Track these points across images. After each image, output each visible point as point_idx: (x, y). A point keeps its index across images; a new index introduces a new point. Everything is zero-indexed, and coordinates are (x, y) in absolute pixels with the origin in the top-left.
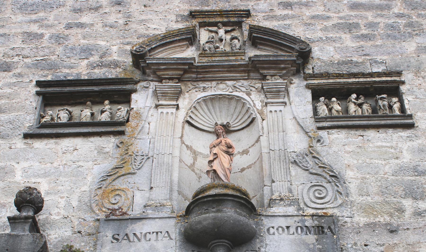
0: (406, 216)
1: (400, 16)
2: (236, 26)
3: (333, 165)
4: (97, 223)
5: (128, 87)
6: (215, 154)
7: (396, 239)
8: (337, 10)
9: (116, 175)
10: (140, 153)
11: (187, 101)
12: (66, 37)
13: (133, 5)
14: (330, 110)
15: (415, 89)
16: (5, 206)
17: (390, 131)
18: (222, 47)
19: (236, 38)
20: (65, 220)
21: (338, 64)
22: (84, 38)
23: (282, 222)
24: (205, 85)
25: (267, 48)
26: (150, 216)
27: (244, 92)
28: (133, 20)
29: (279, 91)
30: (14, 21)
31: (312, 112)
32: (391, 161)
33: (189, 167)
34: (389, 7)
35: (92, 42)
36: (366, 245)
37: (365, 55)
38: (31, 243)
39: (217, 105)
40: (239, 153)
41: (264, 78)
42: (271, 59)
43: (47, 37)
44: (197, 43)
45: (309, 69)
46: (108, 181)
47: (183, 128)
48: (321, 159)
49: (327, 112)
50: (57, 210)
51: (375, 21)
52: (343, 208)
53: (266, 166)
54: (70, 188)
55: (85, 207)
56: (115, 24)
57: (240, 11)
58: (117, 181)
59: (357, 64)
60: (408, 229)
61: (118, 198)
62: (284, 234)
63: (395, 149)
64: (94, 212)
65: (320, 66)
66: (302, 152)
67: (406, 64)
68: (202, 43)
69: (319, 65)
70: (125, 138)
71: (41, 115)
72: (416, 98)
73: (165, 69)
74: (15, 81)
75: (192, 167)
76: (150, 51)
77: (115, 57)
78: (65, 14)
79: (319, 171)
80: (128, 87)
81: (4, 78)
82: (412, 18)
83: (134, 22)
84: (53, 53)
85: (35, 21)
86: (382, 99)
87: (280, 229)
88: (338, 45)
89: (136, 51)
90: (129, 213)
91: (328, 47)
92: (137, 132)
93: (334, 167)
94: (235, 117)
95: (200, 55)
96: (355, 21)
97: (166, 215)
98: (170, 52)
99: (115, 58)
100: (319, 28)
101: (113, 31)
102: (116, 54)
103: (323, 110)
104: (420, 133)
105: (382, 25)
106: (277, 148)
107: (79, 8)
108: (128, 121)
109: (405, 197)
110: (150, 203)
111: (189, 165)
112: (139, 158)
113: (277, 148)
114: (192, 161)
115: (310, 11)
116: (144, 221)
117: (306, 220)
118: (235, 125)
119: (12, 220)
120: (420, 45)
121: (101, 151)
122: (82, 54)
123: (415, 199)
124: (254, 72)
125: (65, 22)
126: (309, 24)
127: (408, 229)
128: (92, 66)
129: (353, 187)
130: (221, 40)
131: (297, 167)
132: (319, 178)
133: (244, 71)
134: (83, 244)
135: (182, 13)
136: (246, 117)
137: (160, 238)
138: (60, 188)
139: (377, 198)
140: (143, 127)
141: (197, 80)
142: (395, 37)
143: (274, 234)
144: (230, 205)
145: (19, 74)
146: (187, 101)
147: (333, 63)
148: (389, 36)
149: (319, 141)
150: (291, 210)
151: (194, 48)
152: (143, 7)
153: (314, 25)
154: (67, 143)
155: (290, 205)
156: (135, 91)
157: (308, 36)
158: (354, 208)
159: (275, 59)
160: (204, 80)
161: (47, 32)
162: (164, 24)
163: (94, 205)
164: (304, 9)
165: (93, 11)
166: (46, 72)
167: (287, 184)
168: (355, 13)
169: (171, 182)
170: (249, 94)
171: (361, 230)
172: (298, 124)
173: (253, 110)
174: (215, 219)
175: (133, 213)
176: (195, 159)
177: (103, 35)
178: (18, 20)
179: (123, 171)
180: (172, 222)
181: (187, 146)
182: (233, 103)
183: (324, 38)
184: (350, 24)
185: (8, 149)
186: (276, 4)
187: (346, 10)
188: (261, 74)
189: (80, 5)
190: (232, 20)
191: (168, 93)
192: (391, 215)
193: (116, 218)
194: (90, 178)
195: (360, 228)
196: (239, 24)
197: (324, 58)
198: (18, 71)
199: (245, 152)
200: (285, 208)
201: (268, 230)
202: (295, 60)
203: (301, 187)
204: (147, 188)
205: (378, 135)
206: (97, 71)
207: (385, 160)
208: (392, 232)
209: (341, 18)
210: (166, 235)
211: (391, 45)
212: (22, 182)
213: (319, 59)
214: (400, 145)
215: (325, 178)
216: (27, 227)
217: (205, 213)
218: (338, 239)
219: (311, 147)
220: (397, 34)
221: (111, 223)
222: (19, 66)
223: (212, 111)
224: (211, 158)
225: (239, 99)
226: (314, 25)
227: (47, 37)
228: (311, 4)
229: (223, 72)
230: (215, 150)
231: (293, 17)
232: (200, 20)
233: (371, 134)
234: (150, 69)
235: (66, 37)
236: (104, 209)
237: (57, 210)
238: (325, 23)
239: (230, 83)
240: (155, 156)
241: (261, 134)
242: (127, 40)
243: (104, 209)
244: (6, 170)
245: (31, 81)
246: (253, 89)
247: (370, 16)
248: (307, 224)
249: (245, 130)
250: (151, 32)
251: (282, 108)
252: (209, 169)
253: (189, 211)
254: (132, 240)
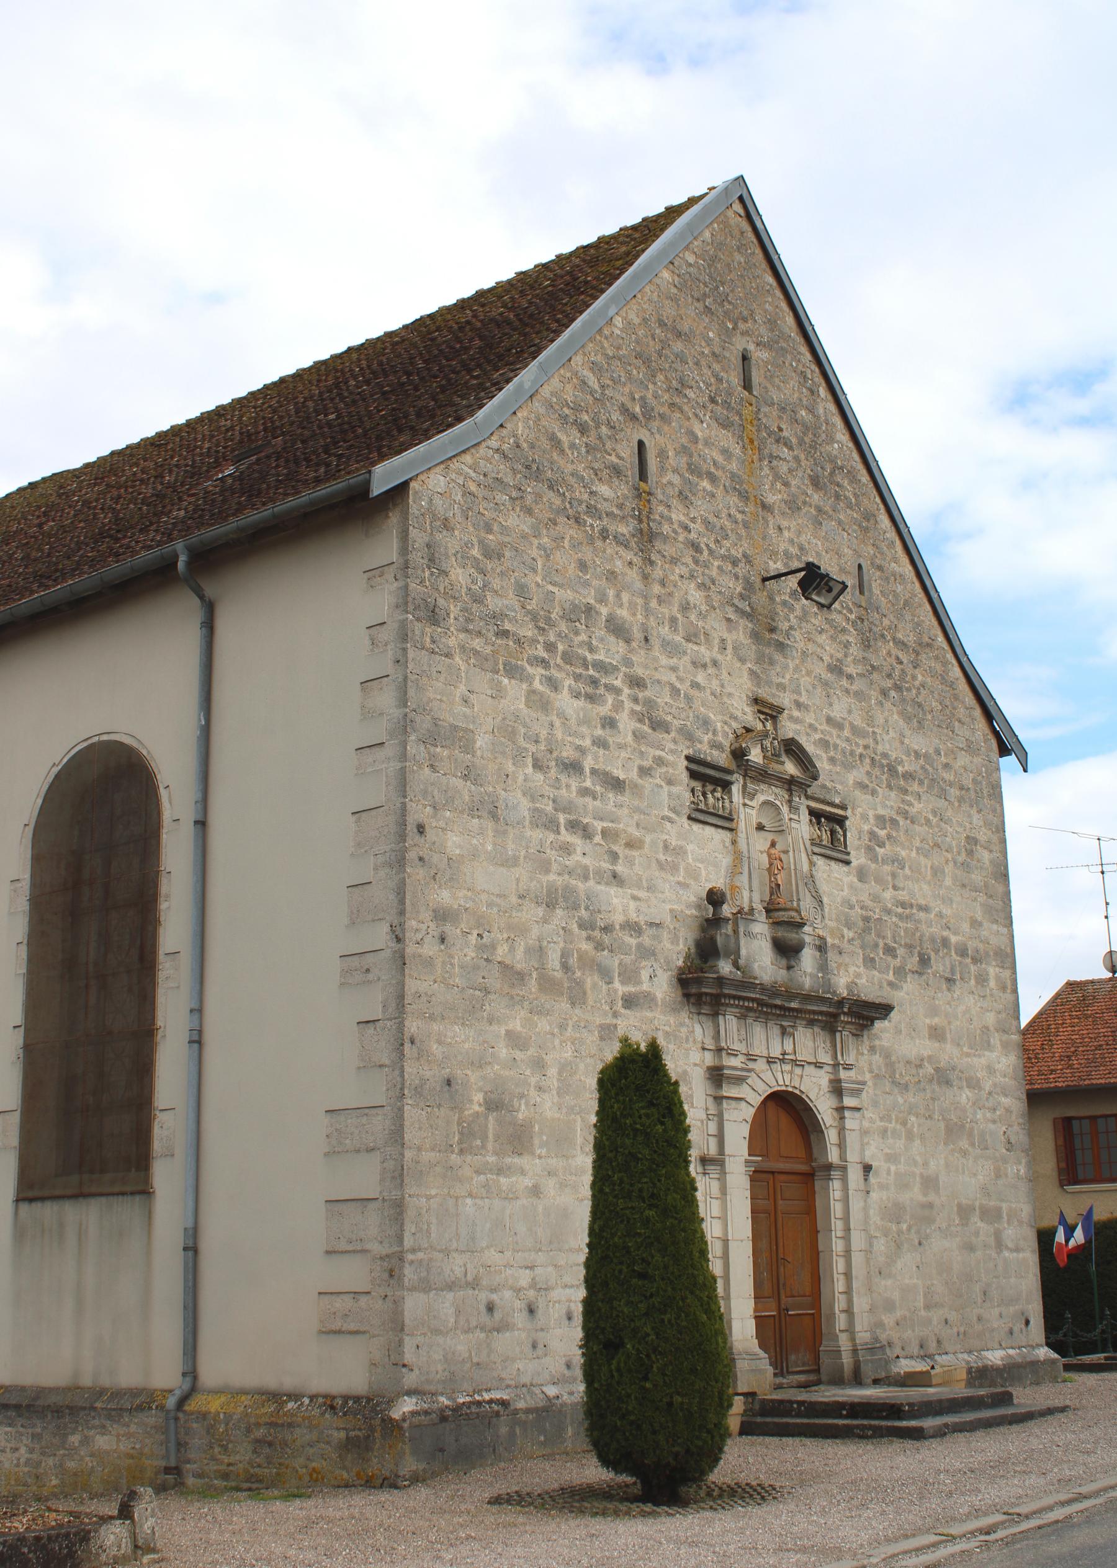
136: (777, 824)
182: (773, 808)
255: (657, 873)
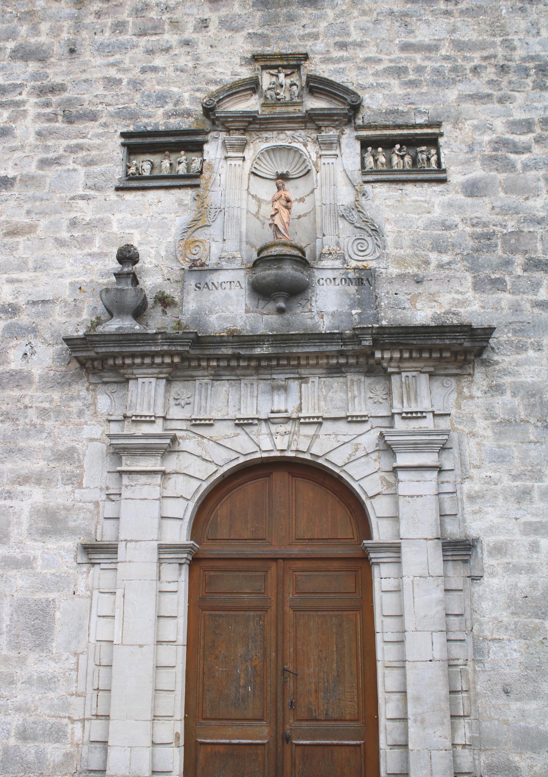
0: (431, 268)
1: (446, 58)
2: (295, 68)
3: (374, 219)
4: (182, 272)
5: (200, 138)
6: (276, 209)
7: (420, 289)
8: (388, 52)
9: (195, 228)
10: (214, 206)
11: (252, 152)
12: (142, 83)
13: (200, 46)
14: (376, 161)
15: (452, 142)
16: (41, 91)
17: (426, 185)
18: (282, 94)
19: (295, 84)
20: (157, 268)
21: (386, 113)
22: (159, 84)
23: (330, 274)
24: (267, 136)
25: (322, 96)
26: (225, 268)
27: (301, 142)
28: (201, 63)
29: (332, 143)
30: (94, 64)
31: (360, 165)
32: (423, 215)
33: (255, 216)
34: (437, 48)
35: (165, 88)
36: (396, 294)
37: (410, 104)
38: (134, 297)
39: (278, 155)
40: (296, 200)
41: (319, 129)
42: (326, 112)
43: (125, 82)
44: (260, 90)
45: (359, 119)
46: (189, 233)
47: (249, 179)
48: (365, 213)
49: (373, 164)
50: (149, 259)
51: (423, 65)
52: (380, 260)
53: (318, 219)
54: (157, 239)
55: (172, 257)
56: (186, 68)
57: (299, 54)
58: (196, 233)
59: (402, 114)
60: (431, 280)
61: (197, 248)
62: (331, 285)
63: (428, 204)
64: (179, 261)
65: (370, 116)
66: (349, 206)
67: (446, 114)
68: (265, 88)
69: (368, 114)
70: (201, 191)
71: (127, 166)
72: (452, 151)
73: (232, 122)
74: (102, 131)
75: (257, 215)
76: (218, 102)
77: (187, 105)
78: (139, 56)
79: (362, 225)
80: (200, 138)
81: (92, 128)
82: (457, 62)
83: (202, 65)
84: (132, 100)
85: (113, 65)
86: (422, 152)
87: (328, 280)
88: (386, 92)
89: (206, 104)
90: (207, 263)
91: (378, 95)
92: (210, 185)
93: (376, 220)
94: (293, 166)
95: (263, 105)
96: (404, 64)
97: (237, 267)
98: (236, 101)
99: (188, 106)
100: (371, 72)
101: (184, 76)
102: (188, 102)
103: (370, 160)
104: (451, 188)
105: (428, 69)
106: (328, 202)
107: (151, 49)
108: (201, 172)
109: (432, 250)
110: (224, 255)
111: (254, 213)
112: (213, 211)
113: (328, 202)
114: (257, 210)
115: (364, 52)
116: (220, 272)
117: (349, 273)
118: (293, 173)
119: (118, 275)
120: (461, 93)
121: (181, 203)
122: (158, 102)
123: (440, 252)
124: (310, 122)
125: (140, 65)
126: (362, 68)
127: (431, 280)
128: (167, 115)
129: (389, 240)
130: (282, 86)
131: (345, 221)
132: (362, 231)
133: (302, 122)
134: (172, 290)
135: (245, 55)
136: (303, 167)
137: (233, 288)
138: (150, 238)
139: (409, 251)
140: (215, 180)
141: (260, 130)
142: (439, 83)
143: (323, 285)
144: (288, 262)
145: (105, 123)
146: (252, 152)
147: (381, 113)
148: (434, 82)
149: (364, 195)
150: (338, 264)
151: (256, 97)
152: (210, 48)
153: (366, 69)
154: (152, 195)
155: (337, 259)
156: (206, 142)
157: (360, 82)
158: (389, 260)
159: (329, 112)
160: (267, 130)
161: (124, 77)
162: (230, 67)
163: (179, 255)
164: (358, 50)
165: (164, 53)
166: (128, 122)
167: (335, 238)
168: (405, 55)
169: (241, 232)
170: (305, 145)
171: (394, 280)
172: (347, 176)
173: (309, 162)
174: (276, 275)
175: (211, 262)
176: (259, 207)
177: (175, 80)
178: (98, 63)
179: (200, 224)
180: (242, 273)
181: (253, 196)
182: (292, 153)
183: (375, 84)
184: (400, 68)
185: (103, 200)
186: (332, 45)
187: (397, 52)
188: (317, 125)
189: (152, 45)
190: (292, 63)
191: (235, 145)
192: (419, 267)
193: (197, 269)
194: (173, 230)
195: (392, 278)
196: (298, 67)
197: (374, 107)
198: (103, 120)
199: (302, 200)
200: (332, 262)
201: (319, 281)
202: (346, 114)
203: (347, 240)
204: (221, 240)
205: (415, 189)
206: (172, 120)
207: (418, 214)
208: (418, 282)
209: (391, 61)
210: (238, 285)
211: (434, 93)
212: (119, 233)
213: (368, 107)
214: (433, 200)
215: (367, 232)
216: (129, 281)
217: (269, 269)
218: (374, 289)
219: (357, 201)
220: (441, 80)
221: (194, 273)
222: (104, 115)
223: (274, 160)
224: (273, 213)
225: (297, 150)
226: (366, 69)
227: (125, 82)
228: (365, 44)
229: (283, 123)
230: (277, 205)
231: (347, 60)
232: (263, 64)
233: (409, 188)
234: (219, 120)
235: (142, 83)
236: (187, 260)
237: (149, 259)
238: (377, 67)
239: (289, 133)
240: (226, 209)
241: (315, 187)
242: (197, 86)
243: (187, 260)
244: (105, 220)
245: (116, 131)
246: (310, 140)
247: (418, 58)
248: (350, 276)
249: (302, 179)
250: (218, 76)
251: (333, 160)
252: (271, 222)
253: (255, 264)
254: (210, 288)
255: (54, 252)
